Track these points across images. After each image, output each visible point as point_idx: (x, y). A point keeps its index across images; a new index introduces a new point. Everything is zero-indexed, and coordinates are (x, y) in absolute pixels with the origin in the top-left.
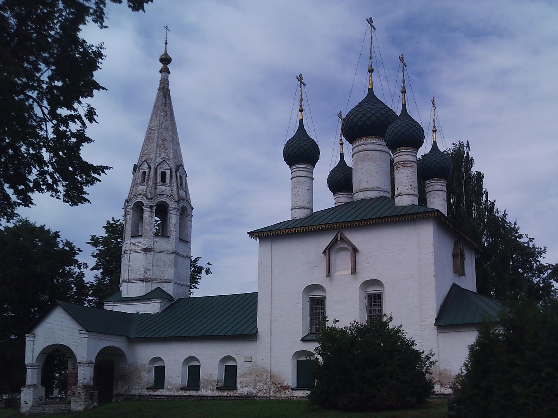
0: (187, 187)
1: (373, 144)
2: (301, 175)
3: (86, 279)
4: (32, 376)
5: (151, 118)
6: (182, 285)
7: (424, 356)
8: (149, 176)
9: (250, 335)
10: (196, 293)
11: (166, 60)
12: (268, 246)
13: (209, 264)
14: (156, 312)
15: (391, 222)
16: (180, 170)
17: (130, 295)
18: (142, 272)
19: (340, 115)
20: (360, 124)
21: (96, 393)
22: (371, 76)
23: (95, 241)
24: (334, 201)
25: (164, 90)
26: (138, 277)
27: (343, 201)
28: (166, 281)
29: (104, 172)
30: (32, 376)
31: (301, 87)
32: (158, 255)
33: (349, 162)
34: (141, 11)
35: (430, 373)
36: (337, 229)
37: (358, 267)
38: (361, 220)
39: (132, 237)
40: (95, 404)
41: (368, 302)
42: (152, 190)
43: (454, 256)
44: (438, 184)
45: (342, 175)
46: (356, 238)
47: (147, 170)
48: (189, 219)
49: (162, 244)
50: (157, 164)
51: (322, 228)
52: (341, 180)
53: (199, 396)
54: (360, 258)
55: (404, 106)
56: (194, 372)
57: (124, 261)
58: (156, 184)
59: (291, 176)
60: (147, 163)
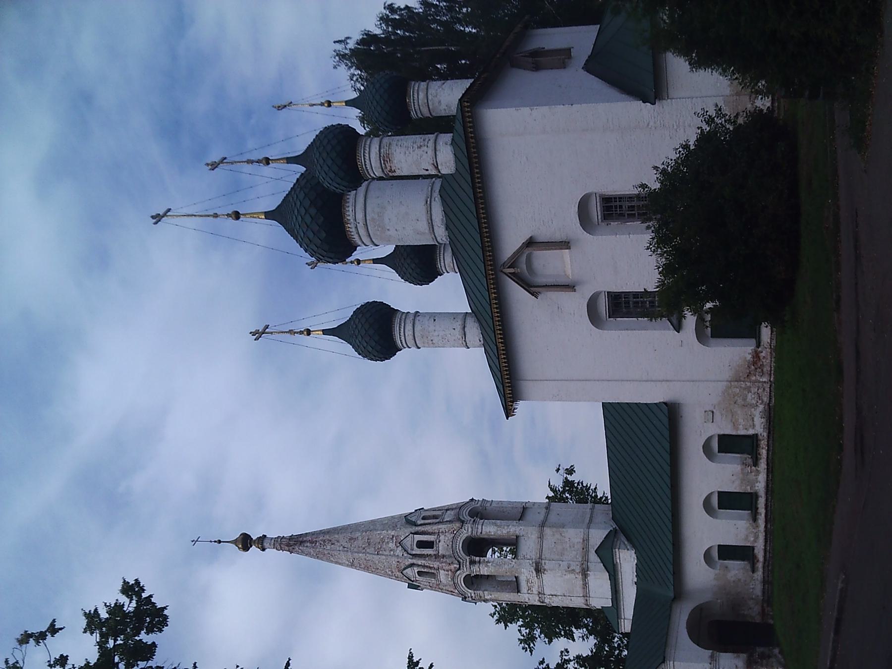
0: (439, 509)
1: (357, 211)
2: (411, 333)
3: (586, 652)
5: (336, 563)
7: (706, 128)
8: (424, 566)
9: (670, 414)
10: (602, 486)
11: (245, 542)
12: (527, 387)
13: (558, 470)
14: (634, 556)
15: (480, 173)
16: (413, 519)
17: (609, 594)
18: (573, 576)
19: (313, 265)
20: (324, 235)
21: (759, 650)
22: (244, 215)
23: (528, 641)
24: (452, 274)
25: (292, 543)
26: (579, 582)
27: (450, 260)
28: (586, 540)
29: (418, 662)
32: (546, 554)
33: (387, 250)
34: (166, 612)
35: (737, 116)
36: (496, 274)
37: (558, 237)
38: (481, 233)
39: (519, 591)
40: (776, 651)
41: (617, 219)
42: (445, 562)
43: (537, 68)
44: (416, 96)
45: (409, 261)
46: (511, 241)
47: (416, 569)
48: (488, 505)
49: (529, 547)
50: (405, 555)
51: (495, 299)
52: (417, 264)
53: (767, 494)
54: (544, 235)
56: (728, 501)
57: (556, 602)
58: (437, 556)
59: (414, 349)
60: (405, 569)
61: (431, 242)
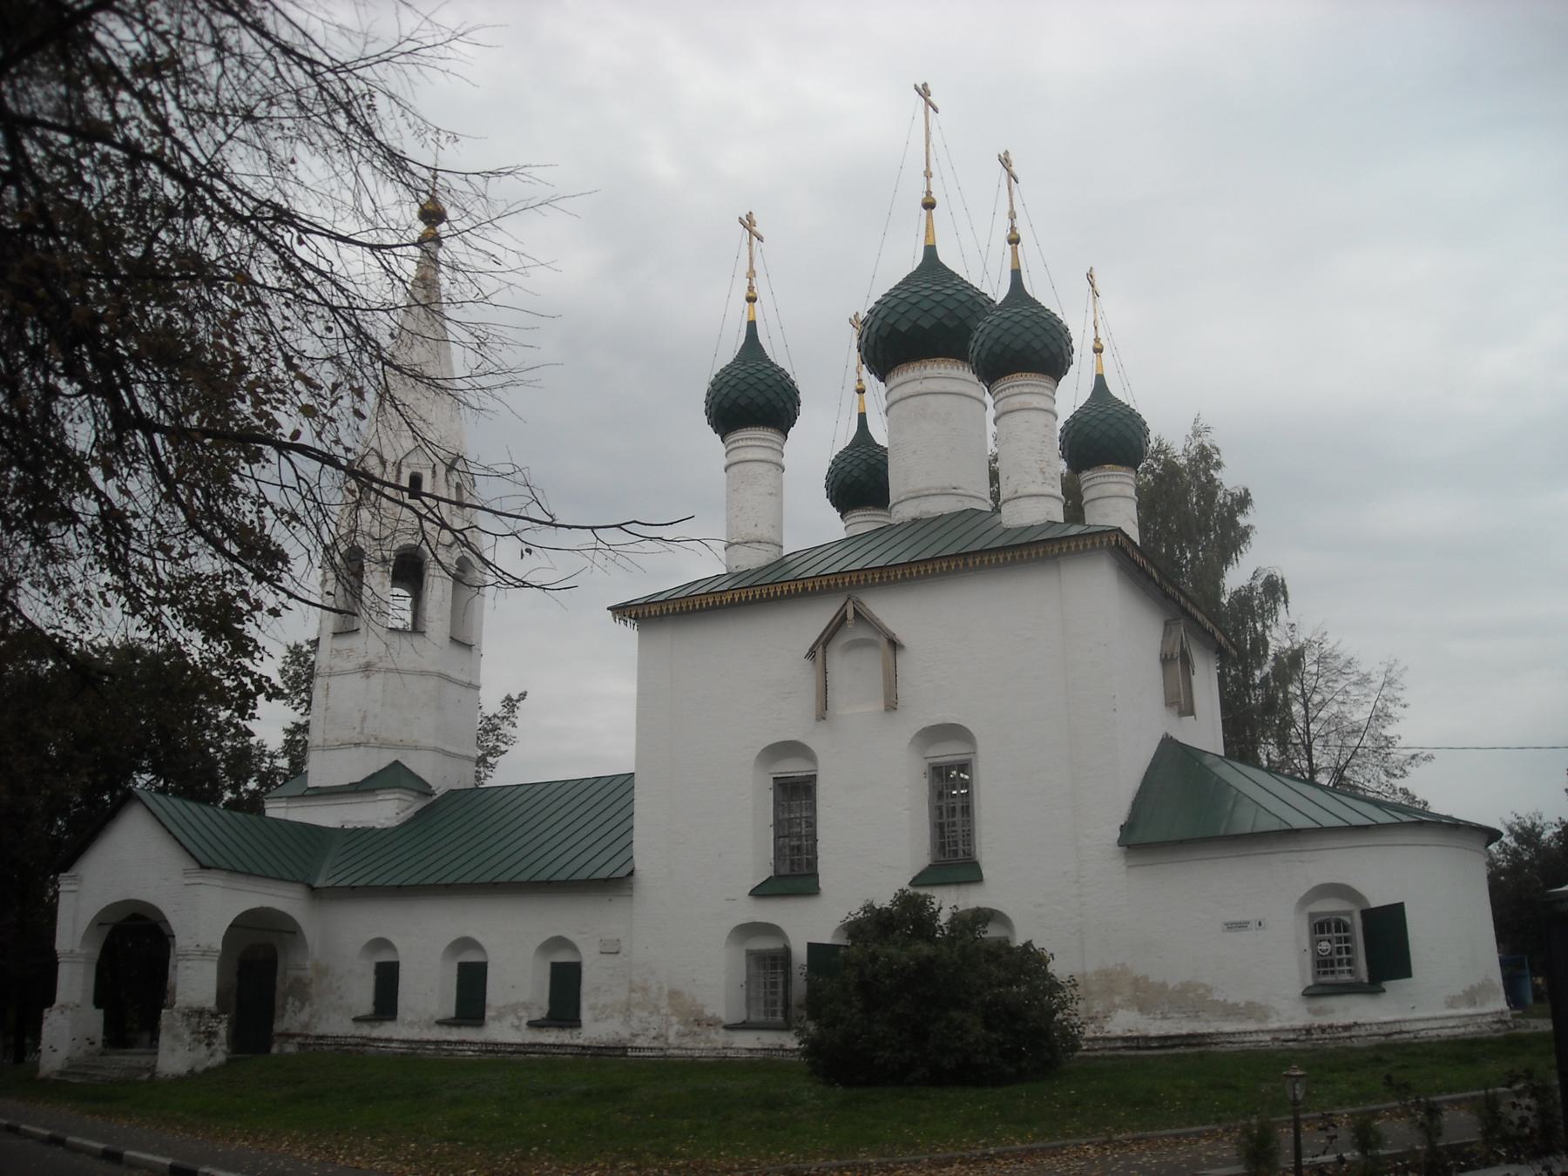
4: (74, 981)
6: (455, 756)
9: (615, 883)
21: (223, 1030)
25: (525, 584)
30: (74, 981)
31: (750, 244)
33: (880, 433)
37: (903, 691)
43: (1166, 660)
49: (407, 653)
51: (805, 589)
52: (859, 480)
54: (907, 664)
55: (1016, 275)
59: (725, 462)
61: (892, 501)
